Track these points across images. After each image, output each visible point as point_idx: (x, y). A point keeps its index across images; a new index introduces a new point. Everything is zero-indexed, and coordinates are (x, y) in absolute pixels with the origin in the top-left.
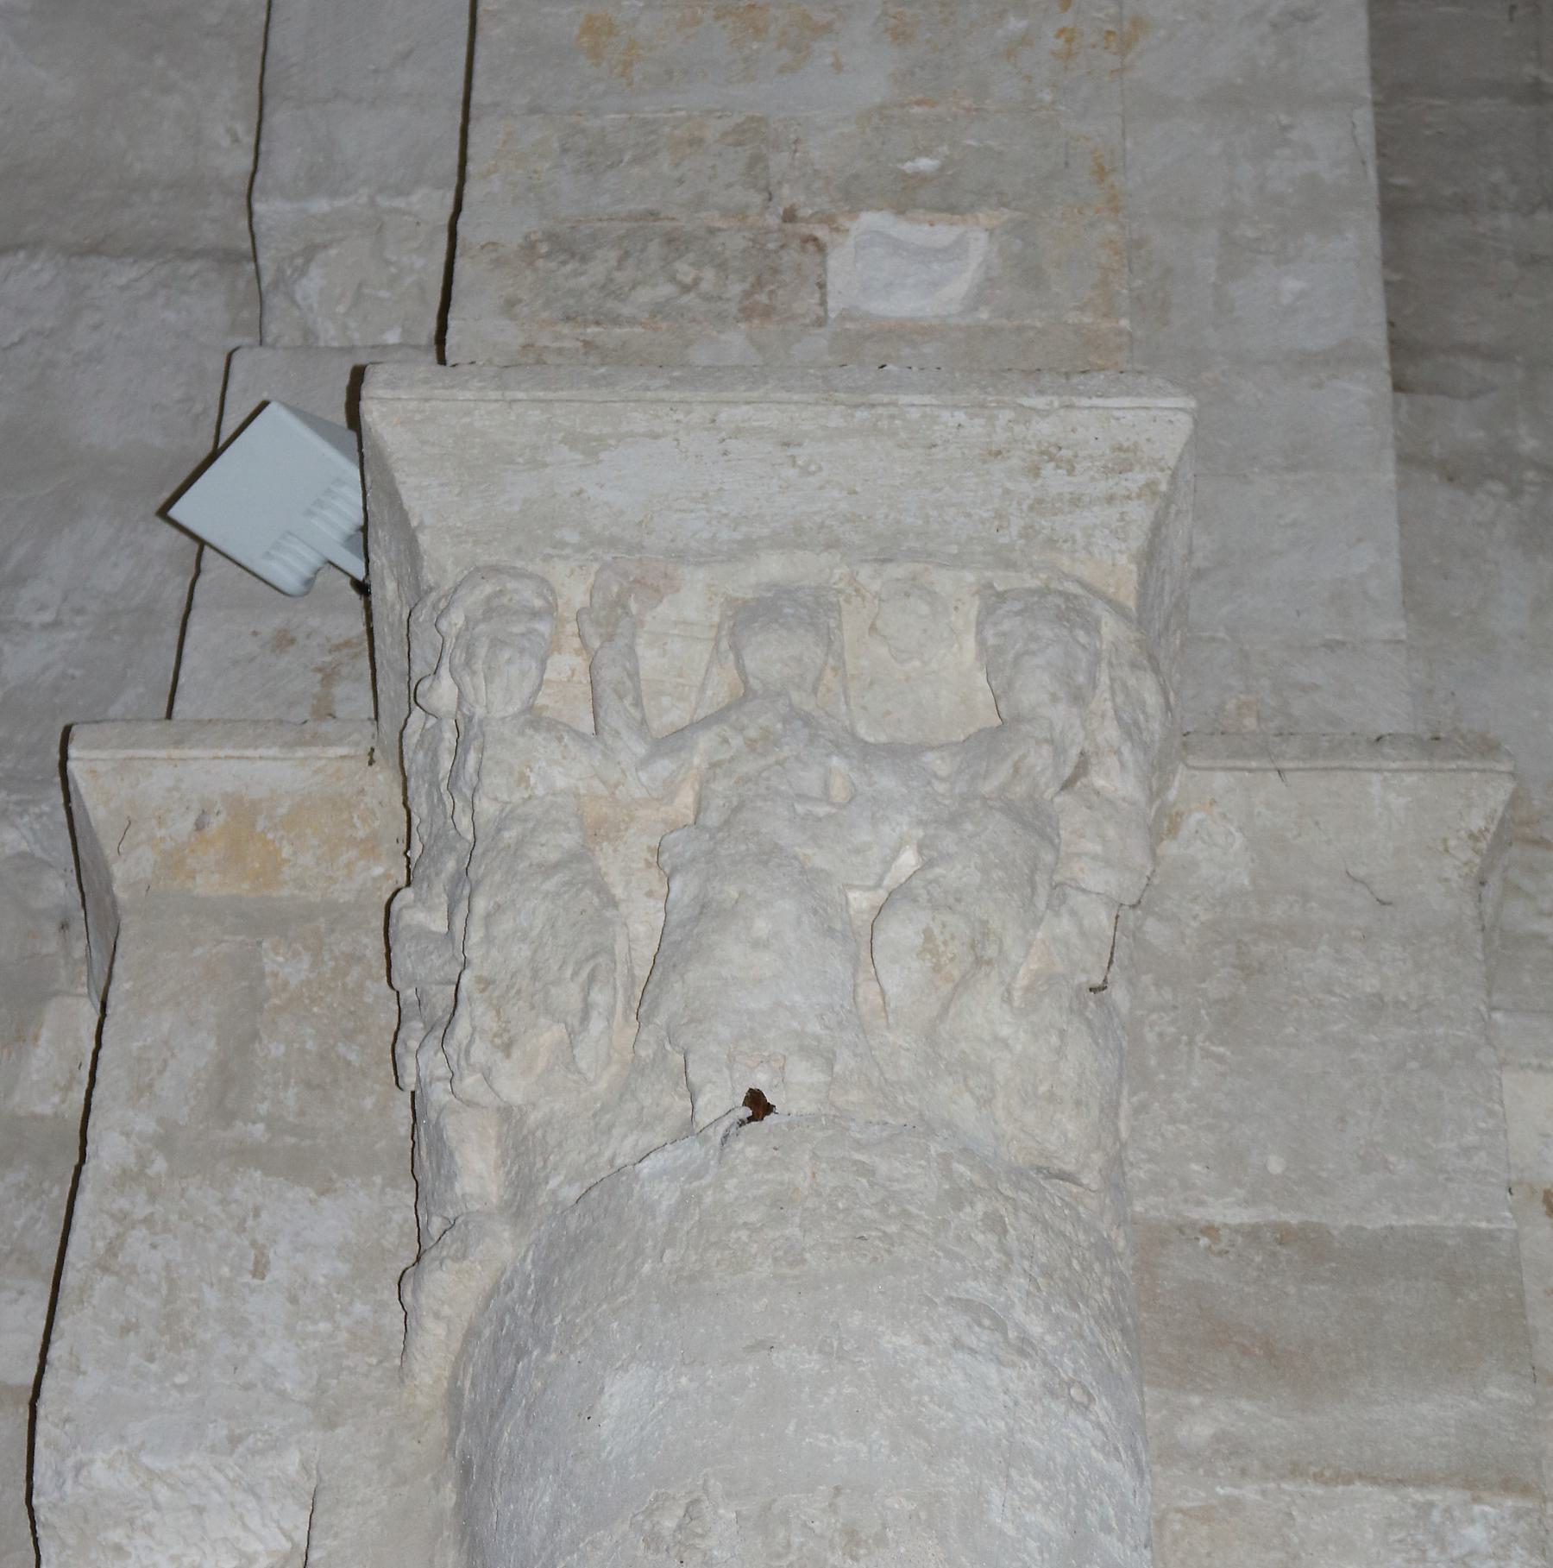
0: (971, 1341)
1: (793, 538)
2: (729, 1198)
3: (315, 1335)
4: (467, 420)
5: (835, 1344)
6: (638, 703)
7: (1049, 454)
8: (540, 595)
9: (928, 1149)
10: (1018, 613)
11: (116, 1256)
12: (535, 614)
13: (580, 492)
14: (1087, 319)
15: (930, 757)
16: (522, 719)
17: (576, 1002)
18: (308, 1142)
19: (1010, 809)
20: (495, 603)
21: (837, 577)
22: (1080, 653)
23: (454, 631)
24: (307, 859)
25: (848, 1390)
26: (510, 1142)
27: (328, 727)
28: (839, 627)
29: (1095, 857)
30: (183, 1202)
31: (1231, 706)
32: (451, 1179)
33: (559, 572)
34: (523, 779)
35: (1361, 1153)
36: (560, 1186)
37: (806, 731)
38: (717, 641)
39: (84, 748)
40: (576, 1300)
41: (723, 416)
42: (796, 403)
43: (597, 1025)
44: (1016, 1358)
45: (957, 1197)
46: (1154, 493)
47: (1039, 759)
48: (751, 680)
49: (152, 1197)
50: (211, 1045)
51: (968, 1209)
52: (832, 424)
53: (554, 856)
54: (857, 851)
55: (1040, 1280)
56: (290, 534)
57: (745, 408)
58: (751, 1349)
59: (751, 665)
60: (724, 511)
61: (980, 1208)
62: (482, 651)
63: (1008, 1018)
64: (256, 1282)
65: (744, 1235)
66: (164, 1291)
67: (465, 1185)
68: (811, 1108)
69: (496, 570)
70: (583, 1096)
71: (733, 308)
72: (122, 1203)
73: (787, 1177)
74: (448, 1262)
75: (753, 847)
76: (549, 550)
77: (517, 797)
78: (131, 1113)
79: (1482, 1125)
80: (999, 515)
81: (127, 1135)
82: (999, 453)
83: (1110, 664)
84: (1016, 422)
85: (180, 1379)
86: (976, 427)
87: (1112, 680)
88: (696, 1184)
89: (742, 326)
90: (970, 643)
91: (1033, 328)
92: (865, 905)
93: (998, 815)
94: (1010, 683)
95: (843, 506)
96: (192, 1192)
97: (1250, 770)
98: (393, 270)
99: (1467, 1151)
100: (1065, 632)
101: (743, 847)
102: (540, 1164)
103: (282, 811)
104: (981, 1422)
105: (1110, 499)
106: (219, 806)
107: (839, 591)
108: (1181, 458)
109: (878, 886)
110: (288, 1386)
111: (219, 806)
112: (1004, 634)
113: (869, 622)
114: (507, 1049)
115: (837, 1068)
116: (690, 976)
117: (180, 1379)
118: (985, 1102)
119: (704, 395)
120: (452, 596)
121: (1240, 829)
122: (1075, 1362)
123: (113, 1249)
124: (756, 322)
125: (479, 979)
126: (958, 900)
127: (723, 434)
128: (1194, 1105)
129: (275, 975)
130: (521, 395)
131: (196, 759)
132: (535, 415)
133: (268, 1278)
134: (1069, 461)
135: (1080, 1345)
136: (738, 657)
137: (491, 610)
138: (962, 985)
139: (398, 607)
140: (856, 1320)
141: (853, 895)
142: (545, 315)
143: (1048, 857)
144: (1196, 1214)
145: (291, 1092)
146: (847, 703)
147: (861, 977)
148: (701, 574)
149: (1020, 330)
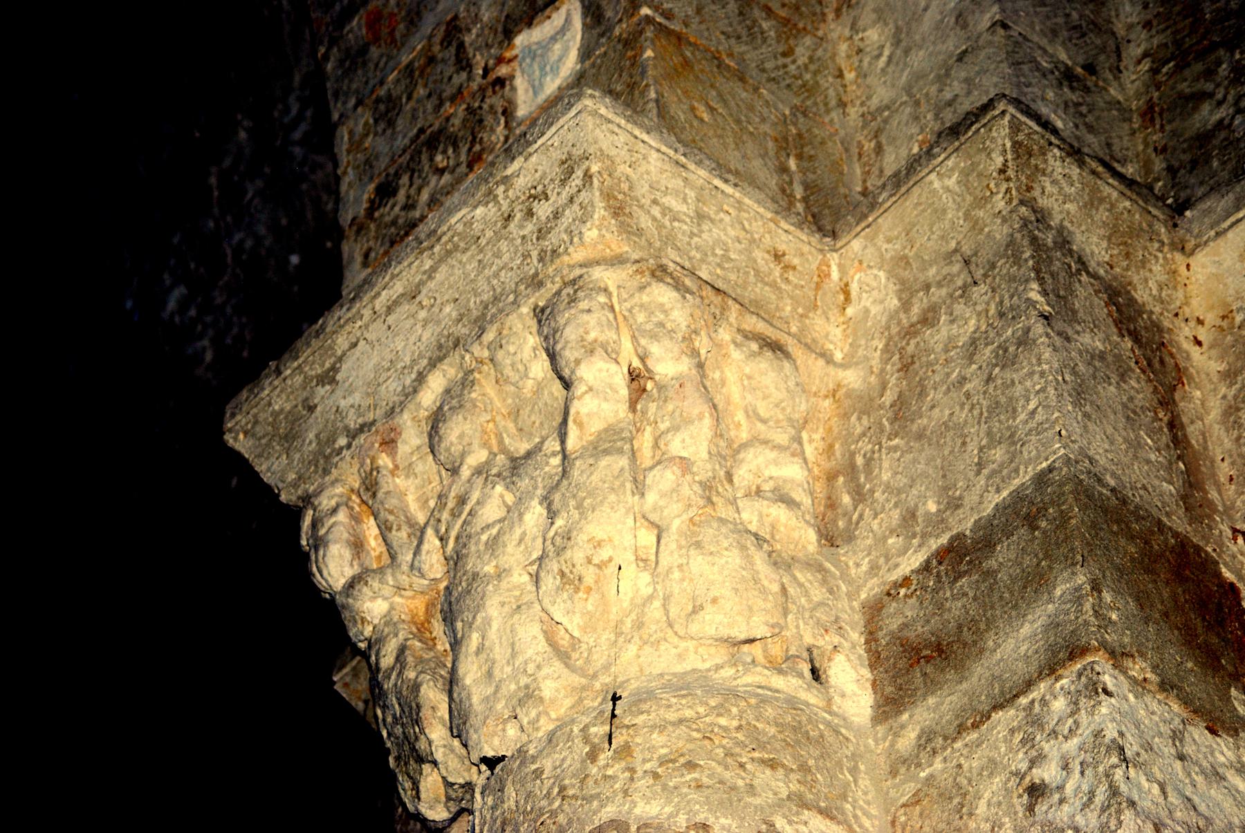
41: (377, 308)
52: (427, 267)
57: (384, 293)
105: (571, 200)
121: (880, 269)
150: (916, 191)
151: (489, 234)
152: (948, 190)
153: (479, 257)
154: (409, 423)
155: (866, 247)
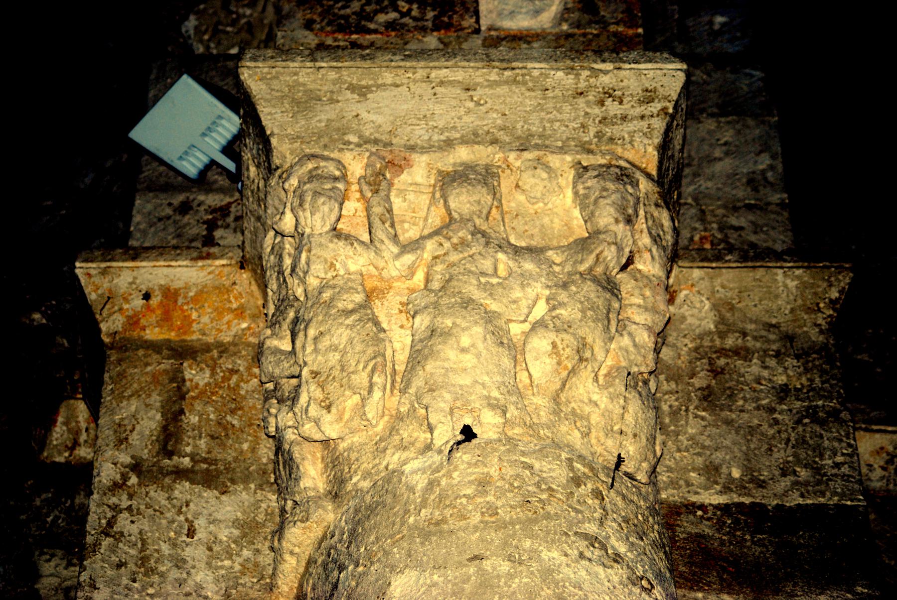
0: (588, 554)
1: (473, 138)
2: (455, 482)
3: (222, 567)
4: (296, 78)
5: (517, 556)
6: (392, 225)
7: (609, 93)
8: (338, 169)
9: (560, 455)
10: (595, 177)
11: (112, 527)
12: (336, 179)
13: (357, 116)
14: (620, 29)
15: (550, 253)
16: (331, 234)
17: (365, 383)
18: (213, 467)
19: (595, 280)
20: (314, 173)
21: (497, 159)
22: (630, 198)
23: (292, 189)
24: (205, 319)
25: (525, 580)
26: (329, 460)
27: (213, 250)
28: (499, 185)
29: (639, 306)
30: (147, 499)
31: (697, 238)
32: (297, 480)
33: (347, 158)
34: (332, 265)
35: (781, 466)
36: (359, 481)
37: (484, 239)
38: (433, 194)
39: (83, 262)
40: (372, 538)
41: (433, 75)
42: (472, 67)
43: (377, 394)
44: (612, 564)
45: (577, 481)
46: (666, 114)
47: (610, 254)
48: (453, 213)
49: (131, 497)
50: (159, 417)
51: (583, 487)
52: (492, 79)
53: (350, 307)
54: (514, 302)
55: (623, 524)
56: (194, 146)
57: (445, 70)
58: (471, 560)
59: (452, 205)
60: (435, 125)
61: (589, 486)
62: (308, 198)
63: (597, 390)
64: (189, 540)
65: (464, 500)
66: (139, 545)
67: (305, 483)
68: (495, 436)
69: (314, 156)
70: (370, 433)
71: (429, 24)
72: (114, 500)
73: (486, 470)
74: (298, 523)
75: (459, 300)
76: (341, 146)
77: (329, 276)
78: (117, 453)
79: (845, 451)
80: (583, 126)
81: (115, 464)
82: (581, 93)
83: (645, 205)
84: (591, 76)
85: (151, 591)
86: (570, 80)
87: (646, 212)
88: (436, 475)
89: (435, 34)
90: (569, 193)
91: (592, 34)
92: (519, 332)
93: (589, 283)
94: (592, 213)
95: (499, 122)
96: (152, 493)
97: (712, 268)
98: (234, 16)
99: (837, 465)
100: (621, 186)
101: (453, 300)
102: (347, 470)
103: (191, 294)
104: (597, 596)
105: (642, 117)
106: (157, 292)
107: (499, 167)
108: (679, 95)
109: (525, 321)
110: (209, 594)
111: (157, 292)
112: (588, 188)
113: (515, 183)
114: (328, 408)
115: (508, 415)
116: (428, 368)
117: (151, 591)
118: (586, 435)
119: (422, 64)
120: (289, 172)
121: (708, 299)
122: (643, 567)
123: (111, 523)
124: (443, 32)
125: (312, 372)
126: (570, 327)
127: (434, 84)
128: (690, 442)
129: (191, 380)
130: (323, 64)
131: (144, 267)
132: (333, 75)
133: (196, 538)
134: (620, 97)
135: (645, 558)
136: (445, 202)
137: (312, 177)
138: (573, 372)
139: (256, 181)
140: (527, 544)
141: (512, 325)
142: (329, 29)
143: (616, 305)
144: (694, 499)
145: (203, 441)
146: (504, 225)
147: (518, 368)
148: (425, 158)
149: (584, 35)
150: (760, 273)
151: (557, 92)
152: (786, 286)
153: (540, 101)
154: (423, 164)
155: (703, 279)
